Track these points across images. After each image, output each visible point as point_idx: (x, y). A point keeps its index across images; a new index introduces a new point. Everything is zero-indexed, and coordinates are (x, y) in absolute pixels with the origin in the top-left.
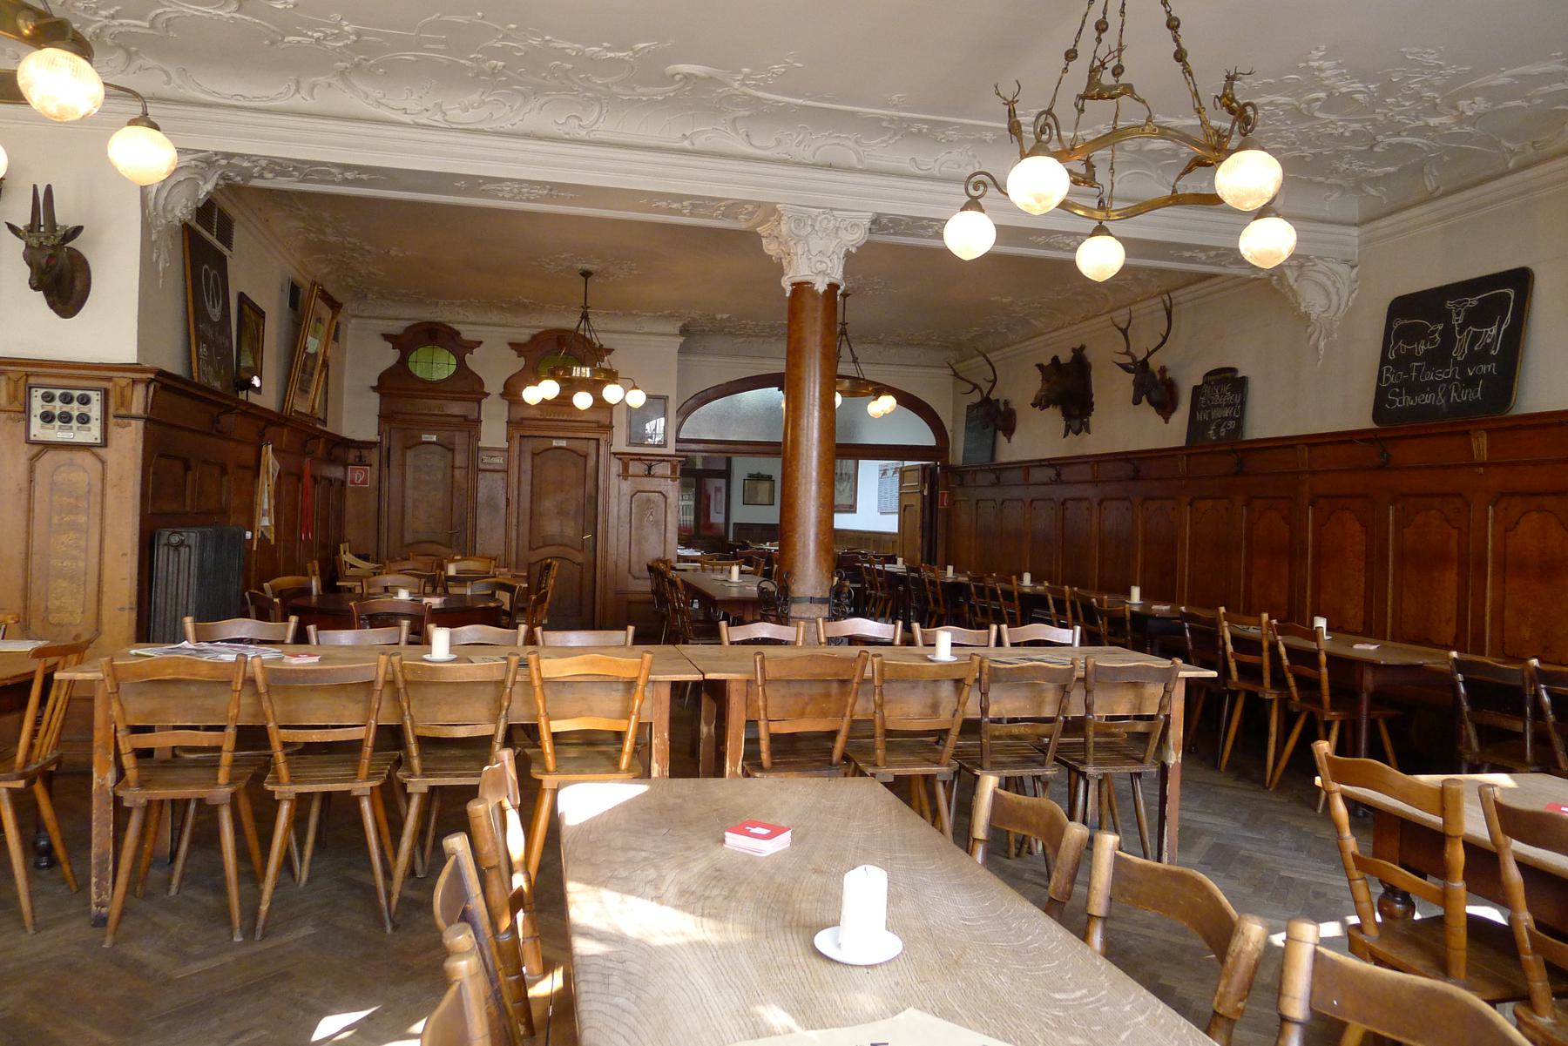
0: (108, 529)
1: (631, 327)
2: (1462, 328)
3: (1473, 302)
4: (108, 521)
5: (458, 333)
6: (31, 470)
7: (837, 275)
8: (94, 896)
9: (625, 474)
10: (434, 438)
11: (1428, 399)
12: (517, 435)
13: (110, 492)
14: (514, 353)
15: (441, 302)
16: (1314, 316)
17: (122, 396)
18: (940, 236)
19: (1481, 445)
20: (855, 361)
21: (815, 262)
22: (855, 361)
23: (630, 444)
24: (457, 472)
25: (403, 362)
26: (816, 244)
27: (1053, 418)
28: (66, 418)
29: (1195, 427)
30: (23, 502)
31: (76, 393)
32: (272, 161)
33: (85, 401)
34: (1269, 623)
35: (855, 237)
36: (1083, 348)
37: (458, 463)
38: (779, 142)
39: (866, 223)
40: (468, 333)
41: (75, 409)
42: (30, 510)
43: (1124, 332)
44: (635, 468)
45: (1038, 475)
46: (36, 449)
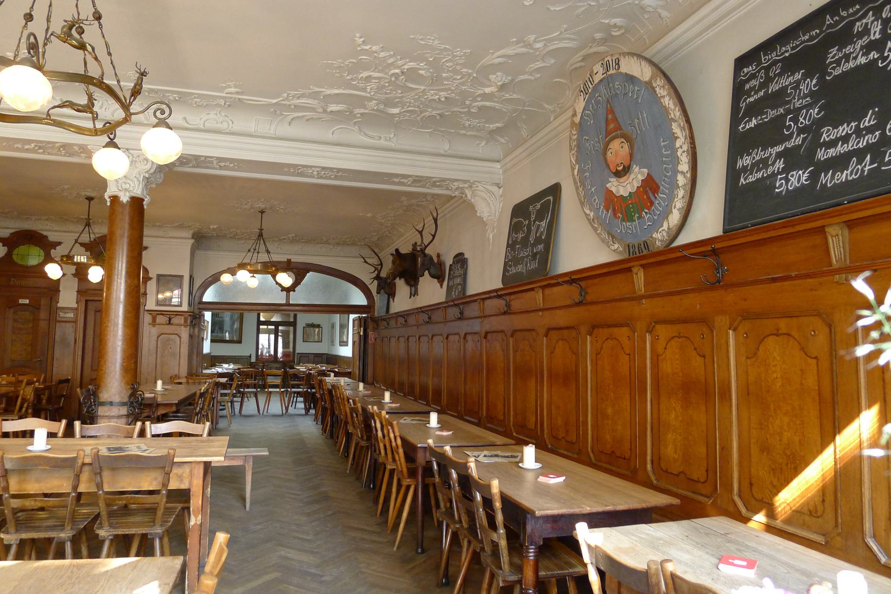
1: (161, 233)
7: (138, 192)
9: (154, 323)
10: (27, 301)
15: (33, 218)
16: (485, 219)
18: (90, 157)
20: (268, 252)
22: (268, 252)
25: (9, 255)
32: (220, 160)
40: (52, 237)
44: (160, 319)
45: (412, 320)
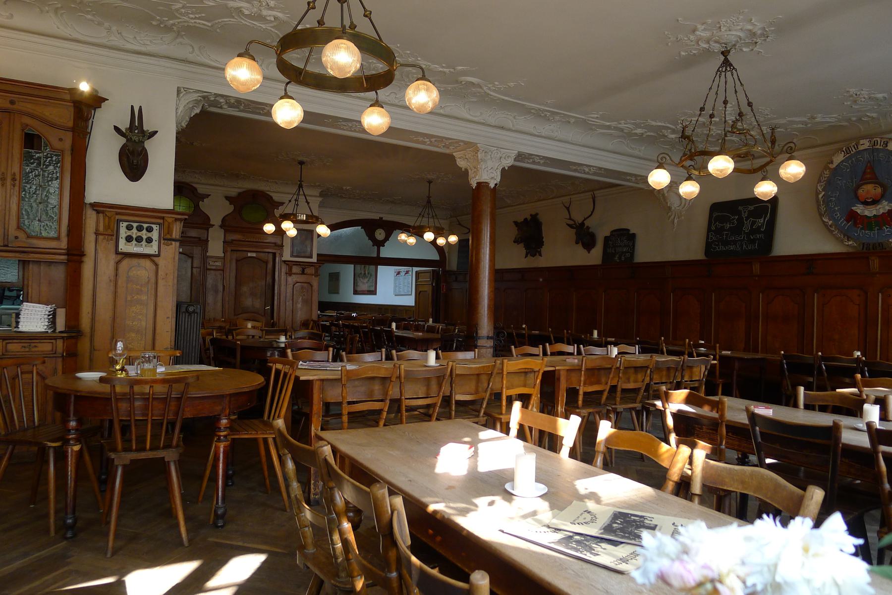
0: (159, 304)
2: (747, 218)
3: (752, 208)
4: (159, 299)
5: (196, 189)
6: (117, 269)
8: (312, 490)
9: (290, 273)
11: (732, 248)
12: (229, 249)
13: (160, 282)
14: (228, 203)
17: (169, 227)
19: (756, 268)
21: (488, 173)
23: (292, 256)
24: (194, 270)
26: (490, 164)
27: (521, 249)
28: (139, 239)
29: (607, 255)
30: (112, 288)
31: (145, 226)
33: (150, 230)
34: (689, 344)
35: (508, 162)
36: (537, 214)
37: (195, 265)
38: (481, 114)
39: (513, 156)
40: (201, 189)
41: (144, 234)
42: (116, 292)
43: (568, 209)
44: (295, 269)
46: (120, 257)
